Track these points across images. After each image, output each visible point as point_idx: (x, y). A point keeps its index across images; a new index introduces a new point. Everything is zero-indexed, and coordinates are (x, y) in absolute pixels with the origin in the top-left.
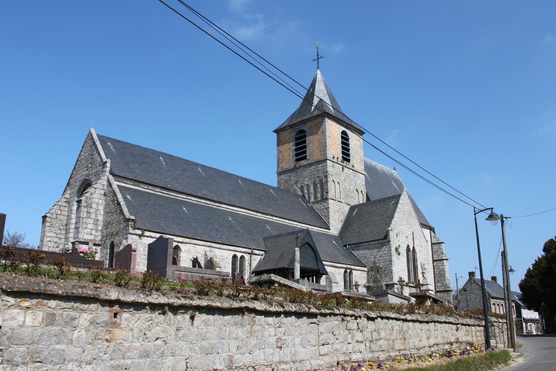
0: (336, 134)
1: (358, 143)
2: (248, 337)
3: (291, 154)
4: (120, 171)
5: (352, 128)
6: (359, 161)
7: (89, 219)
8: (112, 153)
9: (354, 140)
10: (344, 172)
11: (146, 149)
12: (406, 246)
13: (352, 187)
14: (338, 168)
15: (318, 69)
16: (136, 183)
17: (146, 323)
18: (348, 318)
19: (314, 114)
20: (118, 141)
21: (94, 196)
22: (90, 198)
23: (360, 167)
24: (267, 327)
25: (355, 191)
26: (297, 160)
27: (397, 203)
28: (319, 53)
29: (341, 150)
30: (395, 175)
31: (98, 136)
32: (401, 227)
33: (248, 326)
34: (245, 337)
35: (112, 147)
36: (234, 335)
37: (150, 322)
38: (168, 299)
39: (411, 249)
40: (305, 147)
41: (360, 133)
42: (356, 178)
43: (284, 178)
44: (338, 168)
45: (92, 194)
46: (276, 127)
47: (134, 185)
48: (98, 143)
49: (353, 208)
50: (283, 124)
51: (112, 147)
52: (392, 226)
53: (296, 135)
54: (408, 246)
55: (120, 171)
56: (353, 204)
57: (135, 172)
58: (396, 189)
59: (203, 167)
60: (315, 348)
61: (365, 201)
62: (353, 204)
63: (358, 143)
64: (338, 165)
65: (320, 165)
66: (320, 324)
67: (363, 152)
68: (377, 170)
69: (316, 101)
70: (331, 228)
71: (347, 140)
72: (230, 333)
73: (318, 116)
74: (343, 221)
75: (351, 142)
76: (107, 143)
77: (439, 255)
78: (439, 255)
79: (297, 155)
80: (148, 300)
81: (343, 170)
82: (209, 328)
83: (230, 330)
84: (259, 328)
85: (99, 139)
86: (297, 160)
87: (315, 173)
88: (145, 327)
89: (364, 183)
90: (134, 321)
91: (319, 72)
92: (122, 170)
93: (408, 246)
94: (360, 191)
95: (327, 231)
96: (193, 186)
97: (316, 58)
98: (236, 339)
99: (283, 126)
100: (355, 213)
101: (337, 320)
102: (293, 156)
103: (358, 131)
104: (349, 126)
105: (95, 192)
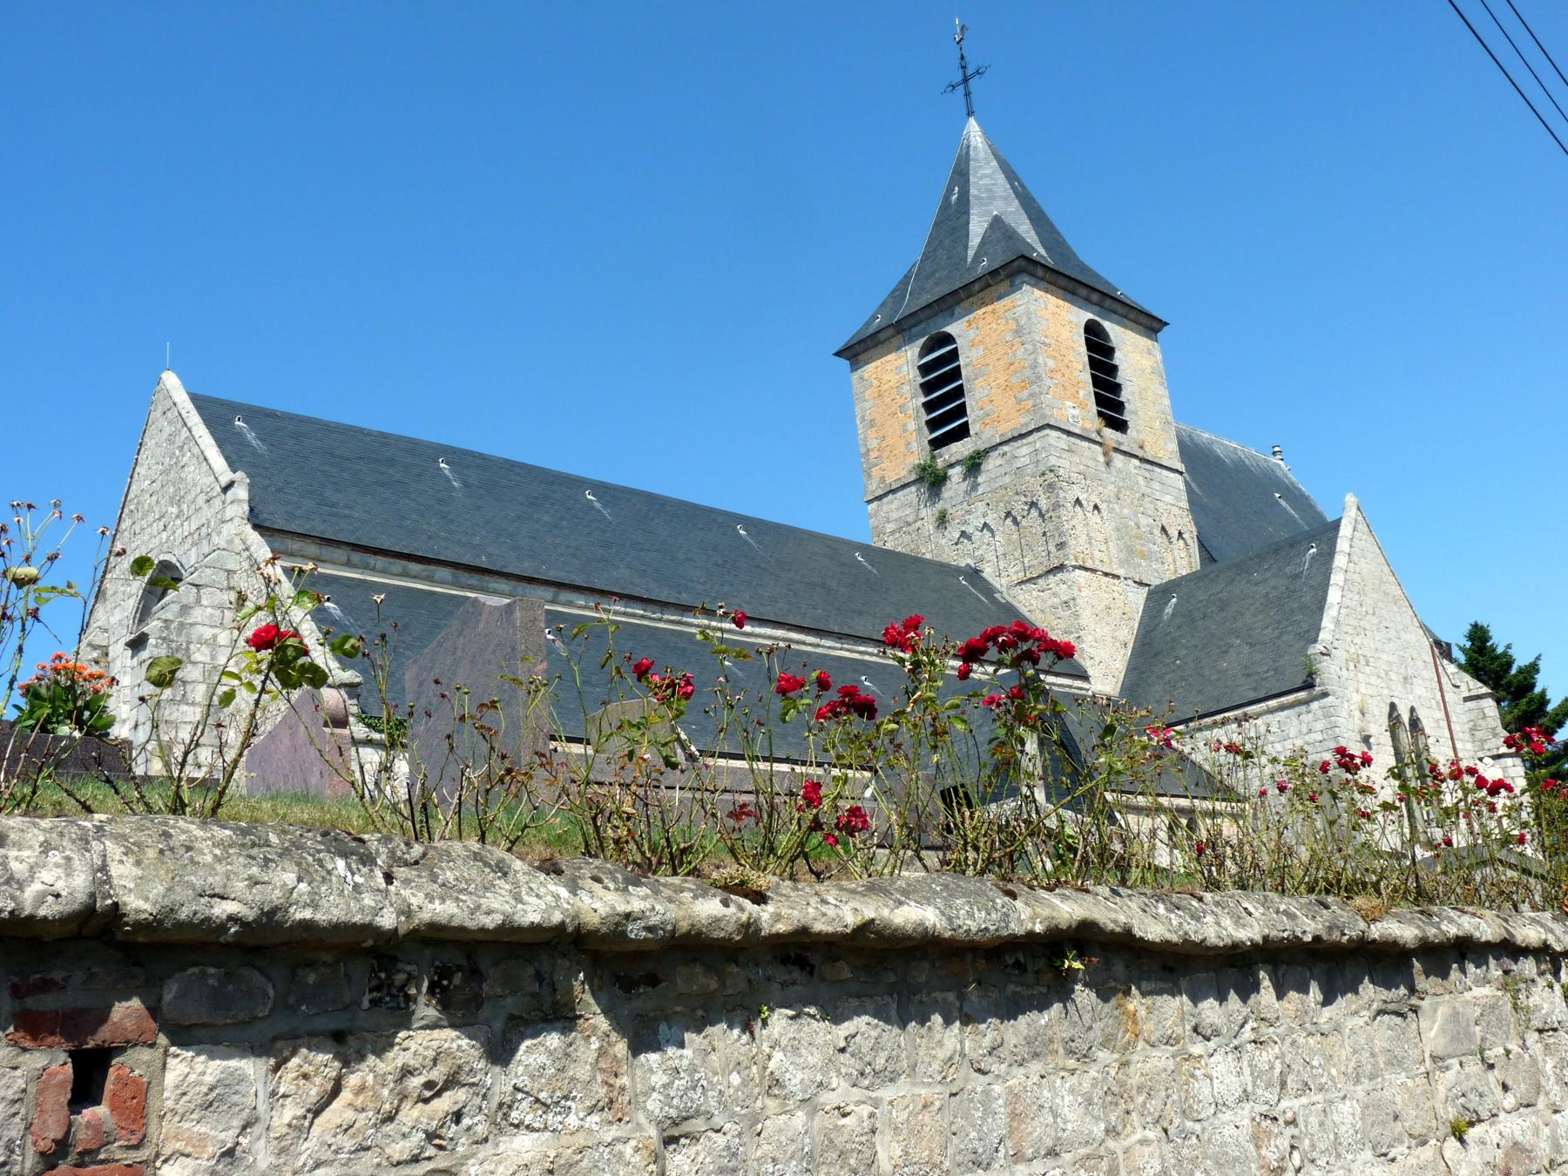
0: (1065, 334)
1: (1147, 363)
2: (1111, 1131)
3: (912, 426)
4: (291, 516)
5: (1119, 308)
6: (1157, 424)
7: (184, 708)
8: (254, 452)
9: (1134, 355)
10: (1113, 470)
11: (383, 438)
12: (1386, 710)
13: (1144, 521)
14: (1088, 453)
15: (970, 113)
16: (357, 557)
17: (411, 1114)
18: (1528, 967)
19: (980, 271)
20: (270, 414)
21: (197, 615)
22: (182, 625)
23: (1168, 451)
24: (1197, 1049)
25: (1157, 532)
26: (936, 444)
27: (1328, 554)
28: (967, 59)
29: (1091, 389)
30: (1279, 473)
31: (196, 399)
32: (1357, 640)
33: (1103, 1055)
34: (1099, 1129)
35: (251, 436)
36: (1038, 1130)
37: (445, 1103)
38: (574, 889)
39: (1406, 718)
40: (959, 392)
41: (1150, 325)
42: (1156, 485)
43: (895, 515)
44: (1088, 453)
45: (185, 609)
46: (840, 344)
47: (349, 564)
48: (194, 419)
49: (1158, 595)
50: (868, 324)
51: (251, 436)
52: (1324, 635)
53: (922, 356)
54: (1393, 706)
55: (291, 516)
56: (1157, 582)
57: (347, 516)
58: (1292, 517)
59: (601, 489)
60: (1427, 1153)
61: (1197, 566)
62: (1155, 582)
63: (1147, 363)
64: (1085, 444)
65: (1024, 451)
66: (1425, 1004)
67: (1166, 393)
68: (1218, 459)
69: (977, 228)
70: (1090, 672)
71: (1109, 351)
72: (1014, 1115)
73: (993, 273)
74: (1130, 646)
75: (1118, 358)
76: (231, 422)
77: (1483, 741)
78: (1483, 741)
79: (933, 425)
80: (407, 912)
81: (1108, 464)
82: (887, 1093)
83: (1014, 1096)
84: (1161, 1059)
85: (198, 408)
86: (936, 444)
87: (1007, 479)
88: (400, 1149)
89: (1185, 505)
90: (290, 1112)
91: (973, 126)
92: (298, 513)
93: (1393, 706)
94: (1174, 533)
95: (1078, 683)
96: (574, 556)
97: (959, 77)
98: (1052, 1153)
99: (871, 331)
100: (1169, 610)
101: (1486, 981)
102: (919, 430)
103: (1142, 318)
104: (1108, 302)
105: (198, 601)
